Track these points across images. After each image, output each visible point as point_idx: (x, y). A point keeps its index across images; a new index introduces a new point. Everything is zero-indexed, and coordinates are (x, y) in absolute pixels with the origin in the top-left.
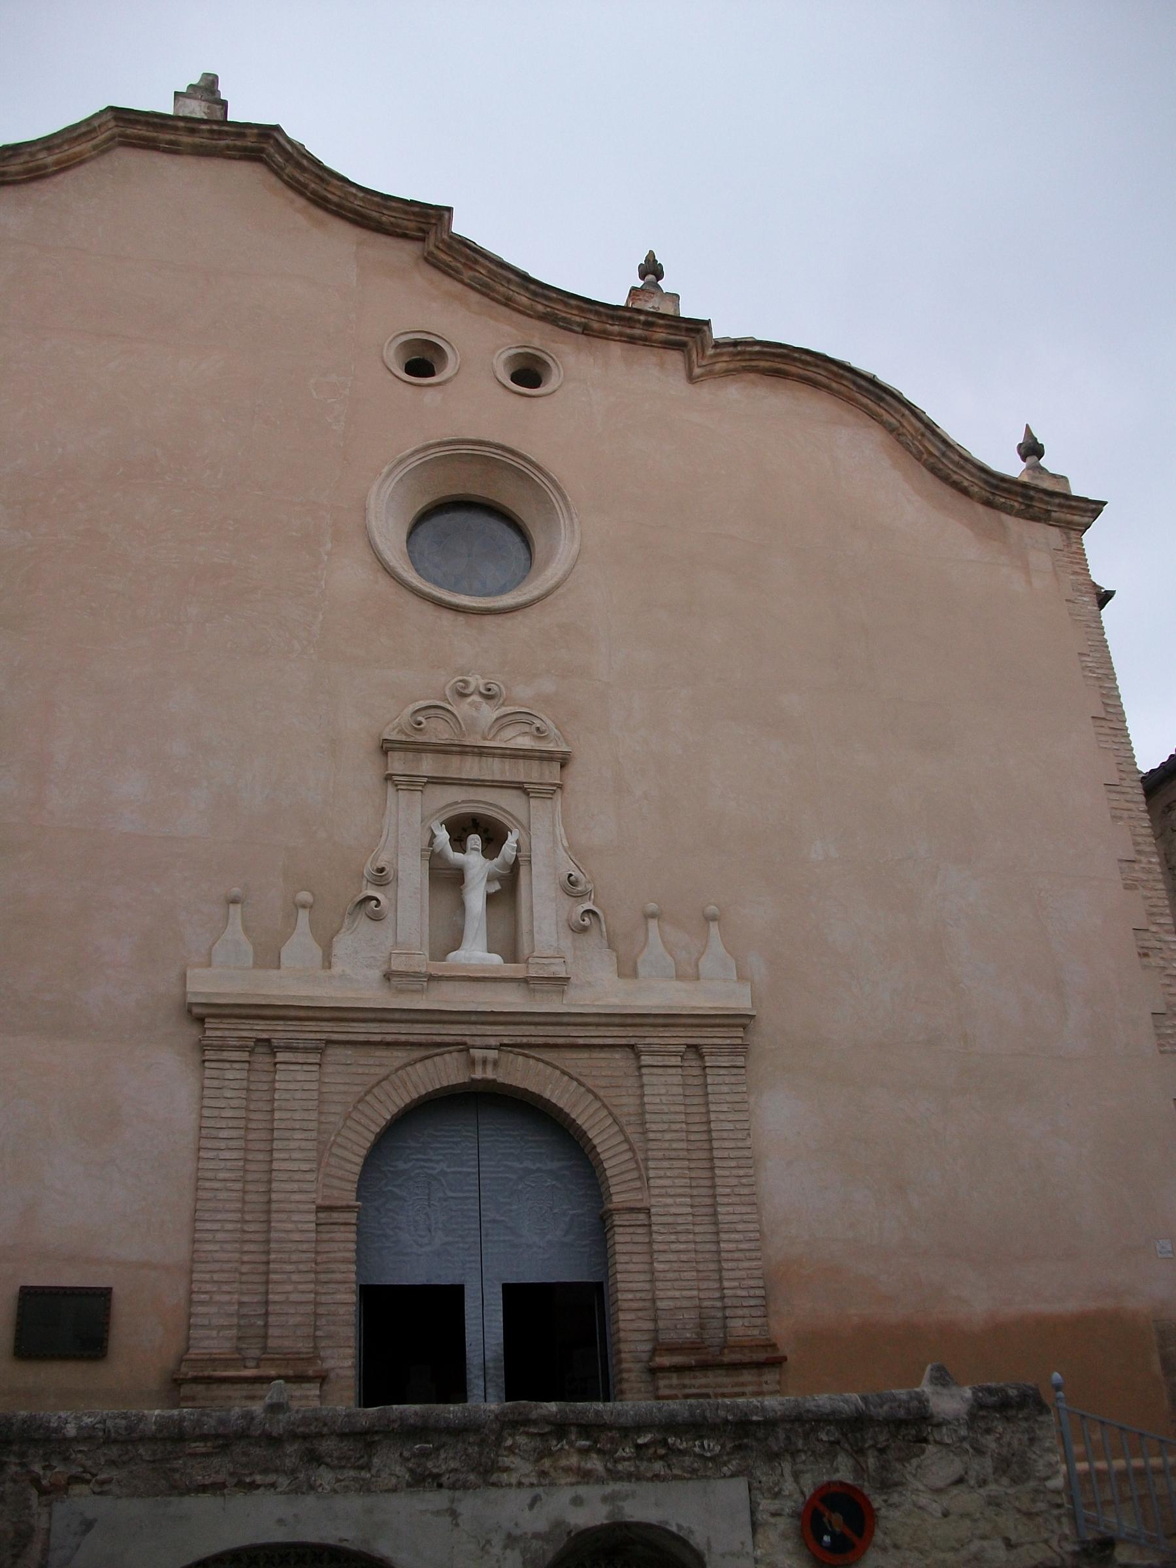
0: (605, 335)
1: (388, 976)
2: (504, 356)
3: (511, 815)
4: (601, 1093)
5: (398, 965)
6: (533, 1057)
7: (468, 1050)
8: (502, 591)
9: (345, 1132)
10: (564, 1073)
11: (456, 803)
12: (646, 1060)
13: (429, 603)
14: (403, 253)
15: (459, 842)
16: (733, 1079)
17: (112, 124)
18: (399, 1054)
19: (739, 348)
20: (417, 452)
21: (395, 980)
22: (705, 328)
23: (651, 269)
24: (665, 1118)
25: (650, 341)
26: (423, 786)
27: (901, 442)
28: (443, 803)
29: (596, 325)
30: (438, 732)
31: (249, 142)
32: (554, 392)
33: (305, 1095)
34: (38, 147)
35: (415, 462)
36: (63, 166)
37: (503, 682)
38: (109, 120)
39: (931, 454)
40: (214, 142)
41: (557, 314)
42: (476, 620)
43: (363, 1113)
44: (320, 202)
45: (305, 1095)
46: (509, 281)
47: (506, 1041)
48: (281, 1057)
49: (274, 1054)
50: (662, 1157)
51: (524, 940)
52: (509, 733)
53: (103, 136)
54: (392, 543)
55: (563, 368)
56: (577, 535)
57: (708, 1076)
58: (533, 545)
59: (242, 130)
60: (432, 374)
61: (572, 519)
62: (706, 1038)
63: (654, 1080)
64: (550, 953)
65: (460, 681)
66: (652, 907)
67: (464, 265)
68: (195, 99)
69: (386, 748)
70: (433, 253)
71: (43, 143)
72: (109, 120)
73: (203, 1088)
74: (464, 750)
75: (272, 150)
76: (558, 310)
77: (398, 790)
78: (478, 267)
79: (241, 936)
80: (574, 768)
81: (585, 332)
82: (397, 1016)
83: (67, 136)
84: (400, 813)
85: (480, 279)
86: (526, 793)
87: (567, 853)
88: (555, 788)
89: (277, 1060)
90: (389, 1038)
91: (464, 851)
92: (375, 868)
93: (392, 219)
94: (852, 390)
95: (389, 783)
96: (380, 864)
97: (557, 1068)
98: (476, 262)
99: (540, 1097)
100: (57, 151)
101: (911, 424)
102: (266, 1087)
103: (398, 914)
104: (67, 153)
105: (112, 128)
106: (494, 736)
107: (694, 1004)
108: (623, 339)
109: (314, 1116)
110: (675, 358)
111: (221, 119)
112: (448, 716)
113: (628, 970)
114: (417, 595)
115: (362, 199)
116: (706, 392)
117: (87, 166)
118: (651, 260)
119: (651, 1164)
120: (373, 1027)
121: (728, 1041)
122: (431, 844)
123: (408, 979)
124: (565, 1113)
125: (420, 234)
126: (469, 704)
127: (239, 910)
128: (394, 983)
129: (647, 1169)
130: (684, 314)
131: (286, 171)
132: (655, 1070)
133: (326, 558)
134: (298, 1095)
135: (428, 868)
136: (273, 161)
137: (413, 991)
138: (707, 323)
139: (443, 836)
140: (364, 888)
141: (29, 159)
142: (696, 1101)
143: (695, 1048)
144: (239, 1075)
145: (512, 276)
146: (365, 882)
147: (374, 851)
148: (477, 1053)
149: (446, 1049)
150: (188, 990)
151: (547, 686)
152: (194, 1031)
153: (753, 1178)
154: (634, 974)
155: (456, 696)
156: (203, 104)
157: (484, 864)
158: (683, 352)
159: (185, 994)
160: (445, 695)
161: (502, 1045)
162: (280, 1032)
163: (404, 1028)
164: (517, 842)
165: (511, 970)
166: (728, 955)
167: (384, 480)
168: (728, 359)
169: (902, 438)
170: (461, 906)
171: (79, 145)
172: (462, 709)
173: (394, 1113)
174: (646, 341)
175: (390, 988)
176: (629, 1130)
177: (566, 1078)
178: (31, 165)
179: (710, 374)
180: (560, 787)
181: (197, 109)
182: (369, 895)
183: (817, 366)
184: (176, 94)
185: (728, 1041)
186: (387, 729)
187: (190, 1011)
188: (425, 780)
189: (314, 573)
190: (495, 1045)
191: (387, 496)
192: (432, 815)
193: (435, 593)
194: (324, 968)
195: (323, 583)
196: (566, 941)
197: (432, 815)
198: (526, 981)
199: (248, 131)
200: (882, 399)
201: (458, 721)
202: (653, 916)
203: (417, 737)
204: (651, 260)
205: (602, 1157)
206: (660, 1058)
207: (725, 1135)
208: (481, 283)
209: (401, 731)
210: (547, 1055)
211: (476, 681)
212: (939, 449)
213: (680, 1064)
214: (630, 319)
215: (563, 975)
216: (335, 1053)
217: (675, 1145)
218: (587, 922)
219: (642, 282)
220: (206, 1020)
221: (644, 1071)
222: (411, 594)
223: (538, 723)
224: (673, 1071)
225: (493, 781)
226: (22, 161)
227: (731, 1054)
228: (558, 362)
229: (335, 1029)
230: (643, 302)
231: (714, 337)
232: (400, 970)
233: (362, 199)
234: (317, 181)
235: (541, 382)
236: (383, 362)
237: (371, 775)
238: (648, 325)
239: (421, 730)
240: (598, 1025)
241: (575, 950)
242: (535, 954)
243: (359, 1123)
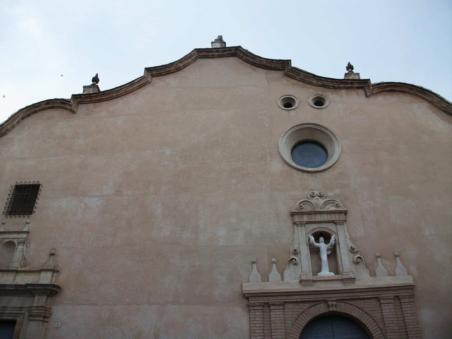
0: (340, 88)
1: (301, 281)
2: (311, 98)
3: (332, 230)
4: (369, 313)
5: (303, 278)
6: (347, 303)
7: (327, 302)
8: (320, 165)
9: (292, 329)
10: (357, 307)
11: (315, 228)
12: (382, 301)
13: (300, 171)
14: (278, 75)
15: (317, 240)
16: (410, 306)
17: (196, 53)
18: (307, 305)
19: (380, 85)
20: (290, 129)
21: (303, 283)
22: (369, 81)
23: (350, 67)
24: (390, 319)
25: (353, 88)
26: (305, 225)
27: (434, 105)
28: (311, 229)
29: (337, 86)
30: (307, 208)
31: (233, 52)
32: (327, 106)
33: (280, 319)
34: (178, 62)
35: (290, 132)
36: (185, 66)
37: (324, 192)
38: (195, 52)
39: (444, 107)
40: (223, 53)
41: (325, 84)
42: (314, 175)
43: (297, 323)
44: (254, 64)
45: (280, 319)
46: (310, 77)
47: (338, 298)
48: (272, 308)
49: (270, 307)
50: (391, 332)
51: (340, 268)
52: (328, 206)
53: (194, 57)
54: (287, 157)
55: (329, 99)
56: (340, 147)
57: (402, 305)
58: (327, 150)
59: (231, 49)
60: (292, 107)
61: (338, 142)
62: (401, 293)
63: (386, 308)
64: (349, 271)
65: (312, 193)
66: (378, 254)
67: (296, 75)
68: (217, 43)
69: (293, 214)
70: (287, 73)
71: (179, 61)
72: (195, 52)
73: (250, 318)
74: (316, 213)
75: (239, 53)
76: (325, 83)
77: (297, 226)
78: (300, 75)
79: (257, 273)
80: (349, 214)
81: (334, 88)
82: (305, 293)
83: (185, 58)
84: (299, 233)
85: (302, 78)
86: (335, 223)
87: (350, 240)
88: (344, 221)
89: (271, 309)
90: (303, 300)
91: (319, 242)
92: (294, 250)
93: (275, 66)
94: (416, 92)
95: (295, 225)
96: (295, 249)
97: (354, 306)
98: (300, 73)
99: (350, 315)
100: (183, 63)
101: (436, 99)
102: (268, 317)
103: (302, 263)
104: (186, 63)
105: (196, 54)
106: (324, 208)
107: (395, 283)
108: (345, 88)
109: (283, 325)
110: (361, 91)
111: (224, 47)
112: (309, 203)
113: (373, 274)
114: (296, 170)
115: (265, 62)
116: (372, 100)
117: (191, 65)
118: (349, 64)
119: (388, 334)
120: (298, 297)
121: (407, 294)
122: (309, 241)
123: (307, 282)
124: (359, 320)
125: (283, 68)
126: (315, 199)
127: (256, 265)
128: (344, 281)
129: (387, 336)
130: (362, 78)
131: (244, 58)
132: (386, 305)
133: (269, 162)
134: (278, 319)
135: (309, 248)
136: (240, 56)
137: (308, 285)
138: (369, 80)
139: (312, 239)
140: (291, 256)
141: (176, 66)
142: (399, 313)
143: (397, 297)
144: (260, 314)
145: (310, 76)
146: (291, 254)
147: (292, 245)
148: (330, 303)
149: (318, 303)
150: (243, 289)
151: (338, 191)
152: (246, 302)
153: (421, 337)
154: (375, 275)
155: (311, 197)
156: (219, 44)
157: (325, 246)
158: (363, 89)
159: (242, 291)
160: (308, 197)
161: (337, 300)
162: (271, 300)
163: (307, 297)
164: (335, 238)
165: (337, 277)
166: (404, 267)
167: (282, 138)
168: (377, 89)
169: (434, 104)
170: (320, 259)
171: (188, 60)
172: (313, 201)
173: (307, 323)
174: (352, 88)
175: (302, 285)
176: (379, 324)
177: (358, 309)
178: (177, 67)
179: (372, 94)
180: (345, 221)
181: (218, 45)
182: (293, 258)
183: (404, 87)
184: (212, 42)
185: (407, 294)
186: (292, 209)
187: (244, 296)
188: (305, 223)
189: (266, 167)
190: (335, 300)
191: (284, 142)
192: (308, 233)
193: (301, 168)
194: (282, 280)
195: (269, 169)
196: (353, 267)
197: (308, 233)
198: (342, 280)
199: (232, 49)
200: (426, 93)
201: (313, 204)
202: (379, 257)
203: (301, 210)
204: (349, 64)
205: (372, 332)
206: (386, 301)
207: (410, 324)
208: (302, 79)
209: (297, 209)
210: (352, 302)
211: (316, 192)
212: (446, 105)
213: (393, 302)
214: (346, 82)
215: (353, 277)
216: (287, 306)
217: (395, 328)
218: (359, 260)
219: (348, 71)
220: (249, 298)
221: (382, 305)
222: (294, 169)
223: (336, 203)
224: (391, 304)
225: (325, 221)
226: (174, 67)
227: (409, 298)
228: (327, 98)
229: (287, 298)
230: (349, 77)
231: (372, 84)
232: (304, 279)
233: (265, 62)
234: (252, 59)
235: (323, 104)
236: (278, 105)
237: (289, 223)
238: (352, 83)
239: (302, 208)
240: (366, 292)
241: (356, 269)
242: (344, 271)
243: (296, 326)
